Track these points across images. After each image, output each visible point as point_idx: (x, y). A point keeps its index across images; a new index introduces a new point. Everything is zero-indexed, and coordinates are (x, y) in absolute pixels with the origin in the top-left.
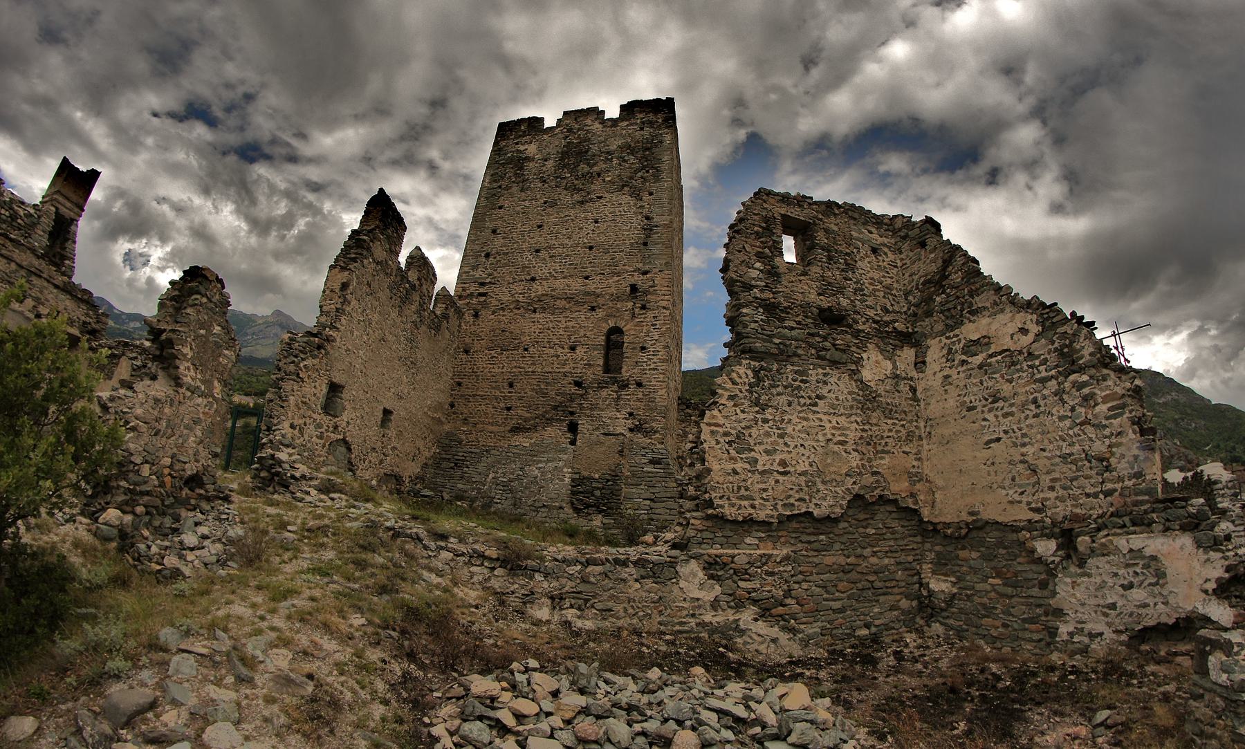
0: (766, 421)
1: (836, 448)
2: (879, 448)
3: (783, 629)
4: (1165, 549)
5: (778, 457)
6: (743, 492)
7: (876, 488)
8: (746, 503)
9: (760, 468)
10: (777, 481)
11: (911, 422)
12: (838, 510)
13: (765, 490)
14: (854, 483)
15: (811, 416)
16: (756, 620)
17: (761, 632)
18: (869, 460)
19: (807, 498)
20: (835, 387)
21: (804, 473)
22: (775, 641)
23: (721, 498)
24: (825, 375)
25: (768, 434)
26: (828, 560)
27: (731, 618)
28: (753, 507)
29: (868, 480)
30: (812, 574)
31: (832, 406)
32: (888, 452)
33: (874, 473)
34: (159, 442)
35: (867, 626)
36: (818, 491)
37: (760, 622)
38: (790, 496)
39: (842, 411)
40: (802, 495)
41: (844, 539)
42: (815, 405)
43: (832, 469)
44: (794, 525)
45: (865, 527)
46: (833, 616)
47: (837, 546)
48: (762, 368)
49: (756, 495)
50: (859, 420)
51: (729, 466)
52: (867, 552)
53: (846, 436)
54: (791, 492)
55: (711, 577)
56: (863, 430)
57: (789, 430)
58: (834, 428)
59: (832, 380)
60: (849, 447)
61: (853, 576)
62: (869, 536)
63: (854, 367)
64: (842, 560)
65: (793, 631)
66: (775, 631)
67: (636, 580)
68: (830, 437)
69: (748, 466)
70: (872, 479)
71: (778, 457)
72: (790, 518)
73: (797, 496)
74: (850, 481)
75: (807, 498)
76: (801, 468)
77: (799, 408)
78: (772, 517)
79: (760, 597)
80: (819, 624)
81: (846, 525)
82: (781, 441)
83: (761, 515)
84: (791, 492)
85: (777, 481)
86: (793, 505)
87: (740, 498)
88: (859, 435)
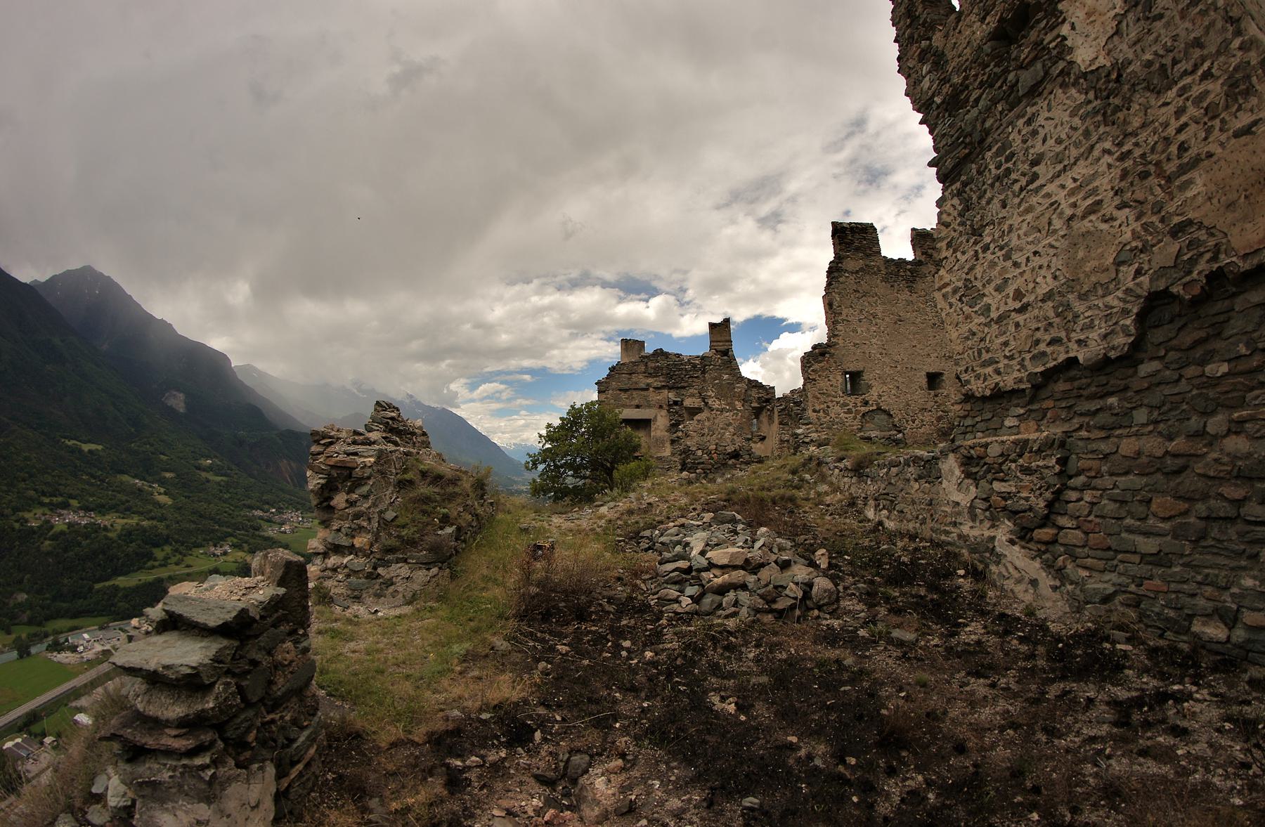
0: (986, 248)
1: (1086, 225)
2: (1170, 168)
3: (1048, 566)
4: (267, 775)
5: (1010, 290)
6: (985, 356)
7: (1193, 261)
8: (990, 370)
9: (994, 315)
10: (1017, 325)
11: (1224, 49)
12: (1121, 340)
13: (1006, 344)
14: (1138, 273)
15: (1034, 200)
16: (1012, 542)
17: (1018, 563)
18: (1158, 208)
19: (1063, 334)
20: (1049, 126)
21: (1049, 296)
22: (1034, 583)
23: (966, 371)
24: (1029, 122)
25: (993, 264)
26: (1128, 446)
27: (987, 534)
28: (998, 372)
29: (1168, 250)
30: (1099, 474)
31: (1058, 158)
32: (1196, 162)
33: (1176, 232)
34: (705, 439)
35: (1231, 620)
36: (1076, 316)
37: (1016, 548)
38: (1037, 342)
39: (1074, 152)
40: (1054, 333)
41: (1155, 398)
42: (1035, 177)
43: (1088, 267)
44: (1061, 386)
45: (1202, 363)
46: (1145, 569)
47: (1141, 416)
48: (965, 184)
49: (999, 355)
50: (1107, 145)
51: (964, 328)
52: (1216, 424)
53: (1095, 191)
54: (1038, 335)
55: (968, 475)
56: (1122, 158)
57: (1014, 242)
58: (1072, 193)
59: (1041, 120)
60: (1108, 209)
61: (1189, 482)
62: (1215, 381)
63: (1061, 65)
64: (1153, 445)
65: (1060, 573)
66: (1034, 568)
67: (916, 480)
68: (1069, 212)
69: (982, 320)
70: (1174, 248)
71: (1010, 290)
72: (1050, 375)
73: (1048, 338)
74: (1128, 272)
75: (1063, 334)
76: (1042, 290)
77: (1017, 201)
78: (1021, 381)
79: (1016, 508)
80: (1113, 577)
81: (1155, 365)
82: (1009, 263)
83: (1008, 382)
84: (1038, 335)
85: (1017, 325)
86: (1044, 354)
87: (984, 365)
88: (1116, 172)
